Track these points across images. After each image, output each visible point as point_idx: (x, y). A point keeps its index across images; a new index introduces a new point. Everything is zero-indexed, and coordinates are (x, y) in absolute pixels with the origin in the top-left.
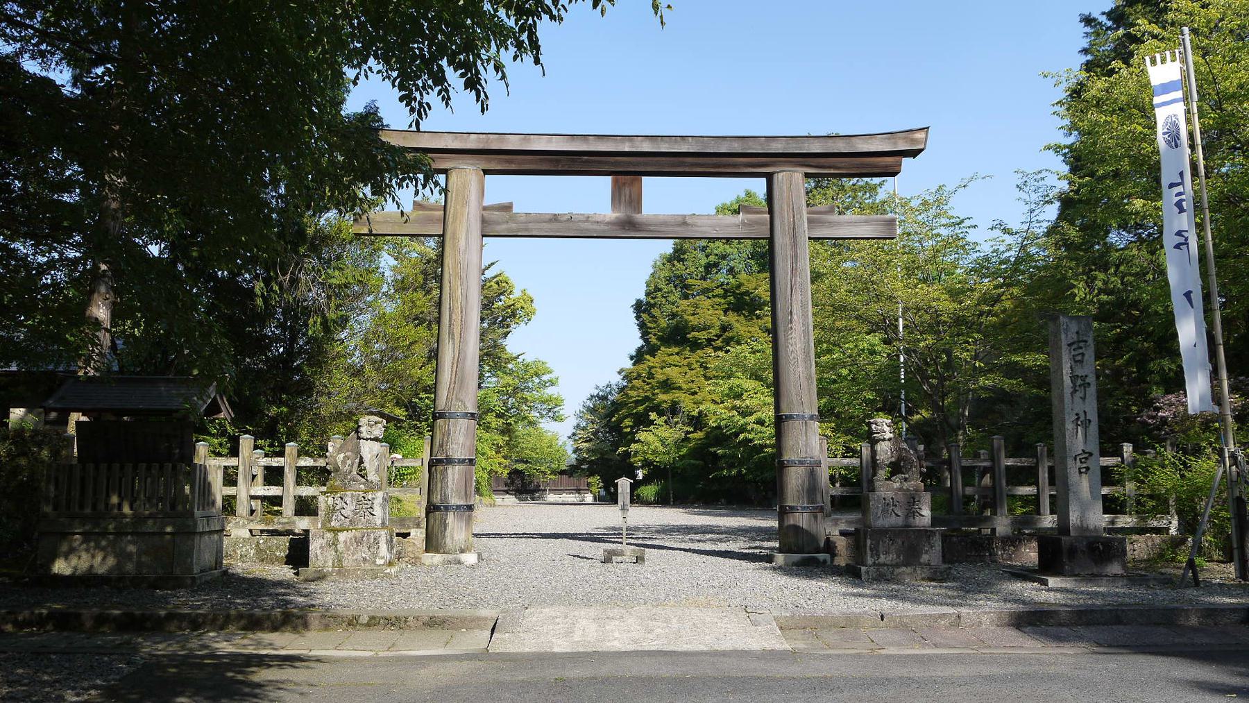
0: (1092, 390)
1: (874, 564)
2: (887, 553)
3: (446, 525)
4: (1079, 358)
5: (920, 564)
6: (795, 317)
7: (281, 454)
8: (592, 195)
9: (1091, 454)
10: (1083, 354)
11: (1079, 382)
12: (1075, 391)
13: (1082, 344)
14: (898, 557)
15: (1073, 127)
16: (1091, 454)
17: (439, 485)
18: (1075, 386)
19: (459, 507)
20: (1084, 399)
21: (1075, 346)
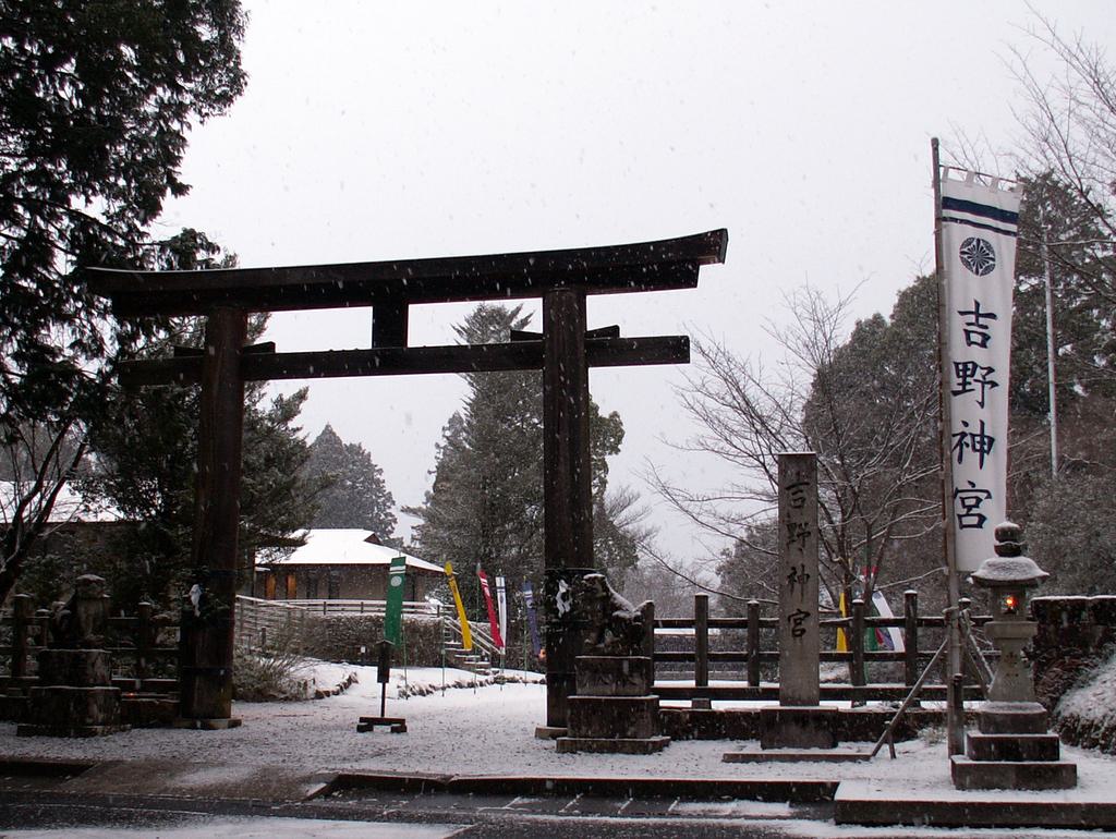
4: (799, 503)
8: (351, 327)
10: (803, 500)
11: (797, 531)
16: (807, 614)
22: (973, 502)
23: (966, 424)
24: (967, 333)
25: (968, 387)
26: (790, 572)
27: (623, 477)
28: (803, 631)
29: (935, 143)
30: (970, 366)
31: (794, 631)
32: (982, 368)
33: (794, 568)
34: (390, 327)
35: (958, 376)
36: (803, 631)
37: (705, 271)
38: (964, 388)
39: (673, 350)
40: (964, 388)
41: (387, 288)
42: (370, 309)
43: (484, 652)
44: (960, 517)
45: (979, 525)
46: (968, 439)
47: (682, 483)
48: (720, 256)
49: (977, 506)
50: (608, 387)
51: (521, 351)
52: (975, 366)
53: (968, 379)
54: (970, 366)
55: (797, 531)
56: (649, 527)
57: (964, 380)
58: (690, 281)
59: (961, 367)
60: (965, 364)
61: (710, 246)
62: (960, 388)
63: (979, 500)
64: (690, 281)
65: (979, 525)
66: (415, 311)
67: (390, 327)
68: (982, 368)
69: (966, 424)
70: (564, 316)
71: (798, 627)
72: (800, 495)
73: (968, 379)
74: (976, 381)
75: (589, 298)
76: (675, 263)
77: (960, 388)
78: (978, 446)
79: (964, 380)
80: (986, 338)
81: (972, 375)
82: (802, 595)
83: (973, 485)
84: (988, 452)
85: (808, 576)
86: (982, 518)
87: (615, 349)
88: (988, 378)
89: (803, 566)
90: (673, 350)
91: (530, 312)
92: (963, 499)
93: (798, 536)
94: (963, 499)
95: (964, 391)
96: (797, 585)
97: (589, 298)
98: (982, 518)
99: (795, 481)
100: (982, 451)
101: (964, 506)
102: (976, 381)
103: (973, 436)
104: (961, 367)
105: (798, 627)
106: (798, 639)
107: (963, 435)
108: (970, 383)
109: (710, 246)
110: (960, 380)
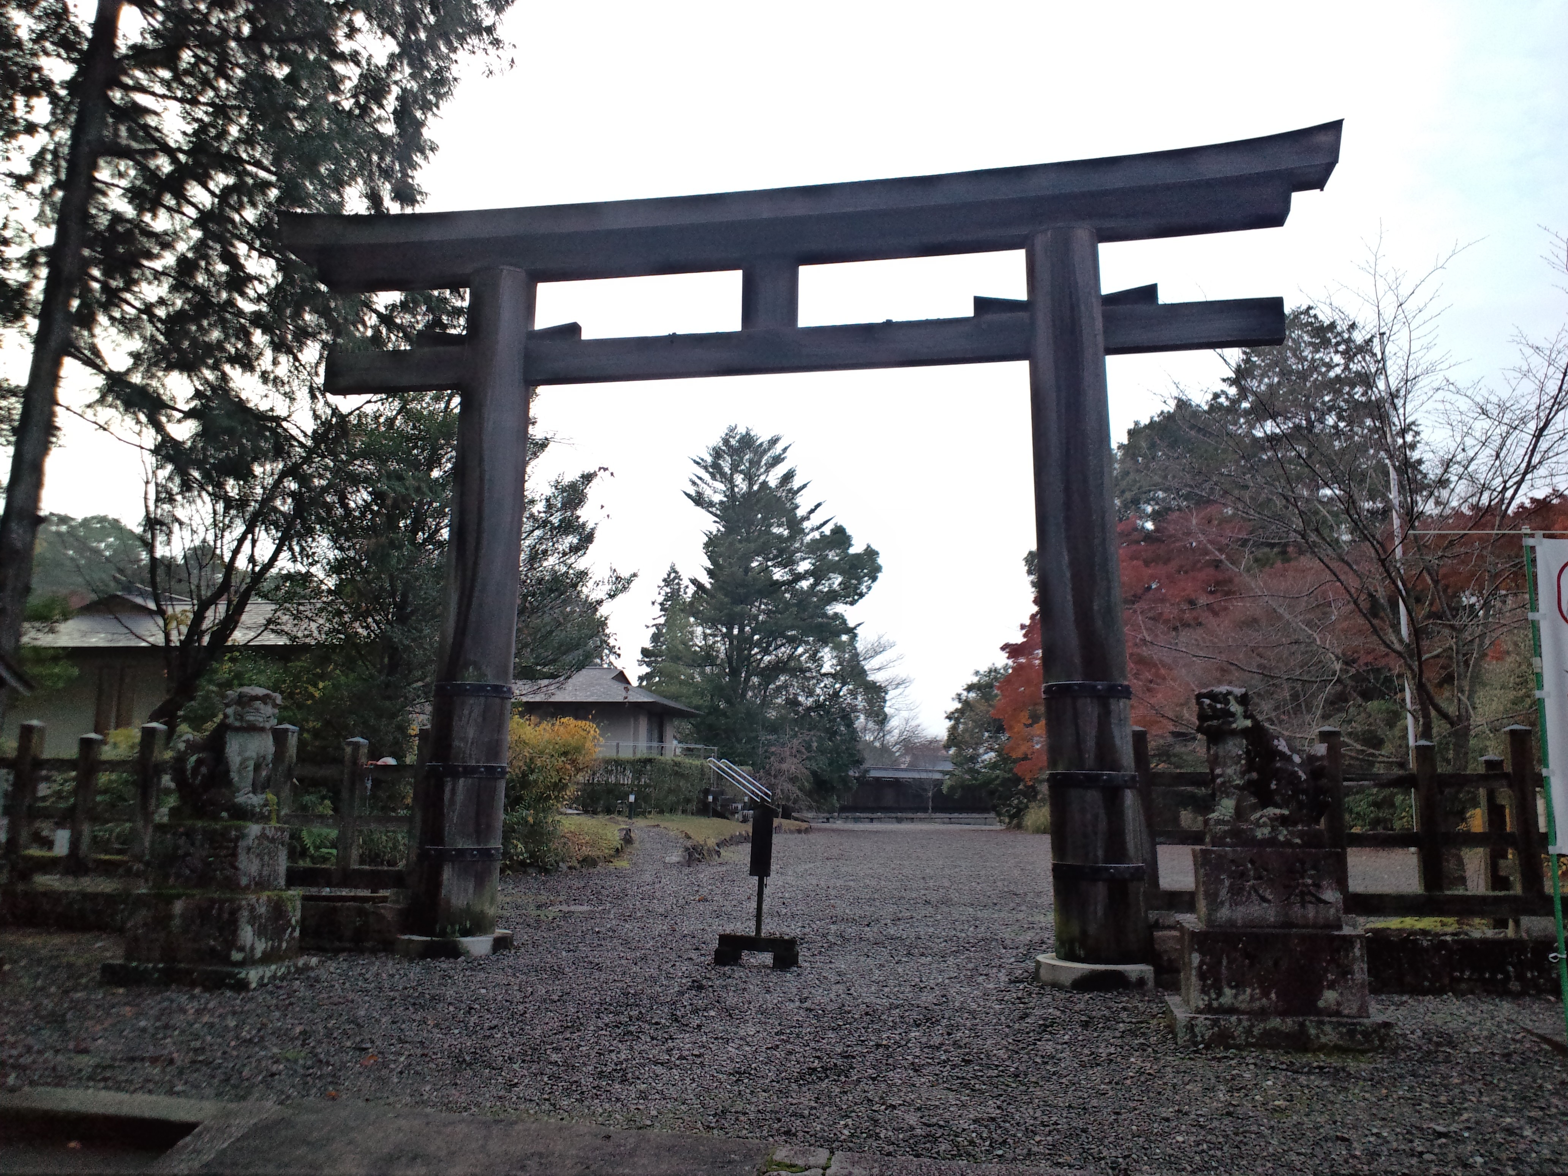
5: (1319, 1012)
14: (1266, 994)
19: (461, 852)
41: (768, 236)
61: (1302, 159)
109: (1302, 159)
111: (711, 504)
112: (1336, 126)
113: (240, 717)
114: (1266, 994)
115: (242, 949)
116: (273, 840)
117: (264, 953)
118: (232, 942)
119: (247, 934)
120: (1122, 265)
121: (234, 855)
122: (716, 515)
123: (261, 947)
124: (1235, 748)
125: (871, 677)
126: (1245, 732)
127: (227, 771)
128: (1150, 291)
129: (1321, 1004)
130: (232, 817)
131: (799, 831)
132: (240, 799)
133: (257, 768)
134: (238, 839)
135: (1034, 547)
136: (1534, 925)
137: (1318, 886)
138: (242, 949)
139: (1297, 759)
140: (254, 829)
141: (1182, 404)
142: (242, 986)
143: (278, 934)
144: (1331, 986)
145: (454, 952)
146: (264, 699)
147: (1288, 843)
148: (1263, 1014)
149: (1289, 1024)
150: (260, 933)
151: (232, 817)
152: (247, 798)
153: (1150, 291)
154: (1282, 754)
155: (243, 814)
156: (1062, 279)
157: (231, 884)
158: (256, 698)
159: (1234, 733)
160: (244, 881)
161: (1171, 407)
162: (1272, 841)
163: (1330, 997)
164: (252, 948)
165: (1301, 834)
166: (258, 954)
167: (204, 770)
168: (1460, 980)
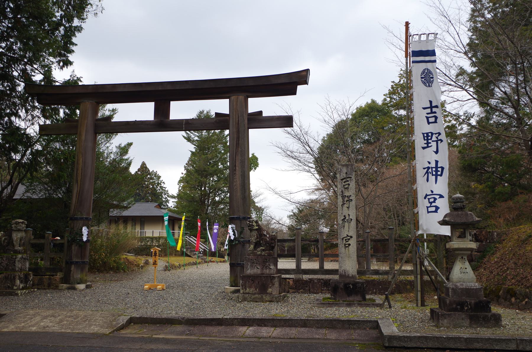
0: (353, 203)
1: (244, 293)
2: (250, 287)
3: (71, 271)
4: (346, 186)
5: (267, 293)
6: (237, 168)
7: (43, 237)
8: (145, 111)
9: (351, 237)
10: (349, 184)
11: (346, 199)
12: (344, 204)
13: (348, 179)
14: (256, 290)
15: (68, 57)
16: (351, 237)
17: (285, 260)
18: (343, 201)
19: (77, 262)
20: (348, 208)
21: (344, 181)
22: (432, 200)
23: (429, 163)
24: (427, 118)
25: (430, 145)
26: (343, 218)
27: (258, 181)
28: (349, 245)
29: (407, 24)
30: (430, 134)
31: (345, 245)
32: (436, 134)
33: (345, 216)
34: (162, 111)
35: (425, 140)
36: (349, 245)
37: (300, 88)
38: (428, 145)
39: (286, 122)
40: (428, 145)
41: (161, 94)
42: (153, 103)
43: (201, 250)
44: (428, 207)
45: (436, 211)
46: (430, 170)
47: (281, 184)
48: (306, 82)
49: (434, 202)
50: (256, 136)
51: (221, 121)
52: (432, 134)
53: (430, 141)
54: (430, 134)
55: (346, 199)
56: (266, 205)
57: (428, 141)
58: (293, 92)
59: (425, 135)
60: (427, 134)
61: (301, 78)
62: (426, 145)
63: (435, 199)
64: (293, 92)
65: (436, 211)
66: (173, 104)
67: (162, 111)
68: (436, 134)
69: (429, 163)
70: (238, 108)
71: (348, 243)
72: (347, 183)
73: (430, 141)
74: (433, 141)
75: (250, 100)
76: (287, 84)
77: (426, 145)
78: (434, 173)
79: (428, 141)
80: (436, 118)
81: (431, 139)
82: (349, 228)
83: (432, 192)
84: (441, 175)
85: (351, 220)
86: (437, 208)
87: (259, 120)
88: (439, 138)
89: (349, 215)
90: (286, 122)
91: (221, 106)
92: (429, 199)
93: (347, 201)
94: (429, 199)
95: (428, 147)
96: (346, 224)
97: (250, 100)
98: (437, 208)
99: (345, 177)
100: (436, 175)
101: (429, 202)
102: (433, 141)
103: (432, 168)
104: (425, 135)
105: (348, 243)
106: (347, 248)
107: (428, 168)
108: (430, 143)
109: (301, 78)
110: (426, 142)
111: (194, 141)
112: (307, 71)
113: (16, 227)
114: (256, 290)
115: (16, 286)
116: (25, 259)
117: (22, 287)
118: (14, 285)
119: (18, 282)
120: (255, 104)
121: (15, 262)
122: (195, 145)
123: (21, 286)
124: (255, 233)
125: (256, 205)
126: (256, 229)
127: (13, 241)
128: (261, 112)
129: (268, 292)
130: (14, 253)
131: (221, 262)
132: (16, 248)
133: (21, 240)
134: (15, 258)
135: (252, 173)
136: (42, 241)
137: (269, 265)
138: (16, 286)
139: (268, 236)
140: (20, 256)
141: (373, 101)
142: (17, 294)
143: (26, 282)
144: (270, 288)
145: (74, 289)
146: (22, 223)
147: (264, 255)
148: (255, 294)
149: (260, 296)
150: (21, 282)
151: (14, 253)
152: (18, 248)
153: (261, 112)
154: (264, 235)
155: (17, 252)
156: (238, 108)
157: (14, 270)
158: (20, 222)
159: (254, 230)
160: (17, 269)
161: (370, 102)
162: (260, 255)
163: (270, 290)
164: (19, 286)
165: (267, 253)
166: (21, 287)
167: (6, 241)
168: (323, 290)
